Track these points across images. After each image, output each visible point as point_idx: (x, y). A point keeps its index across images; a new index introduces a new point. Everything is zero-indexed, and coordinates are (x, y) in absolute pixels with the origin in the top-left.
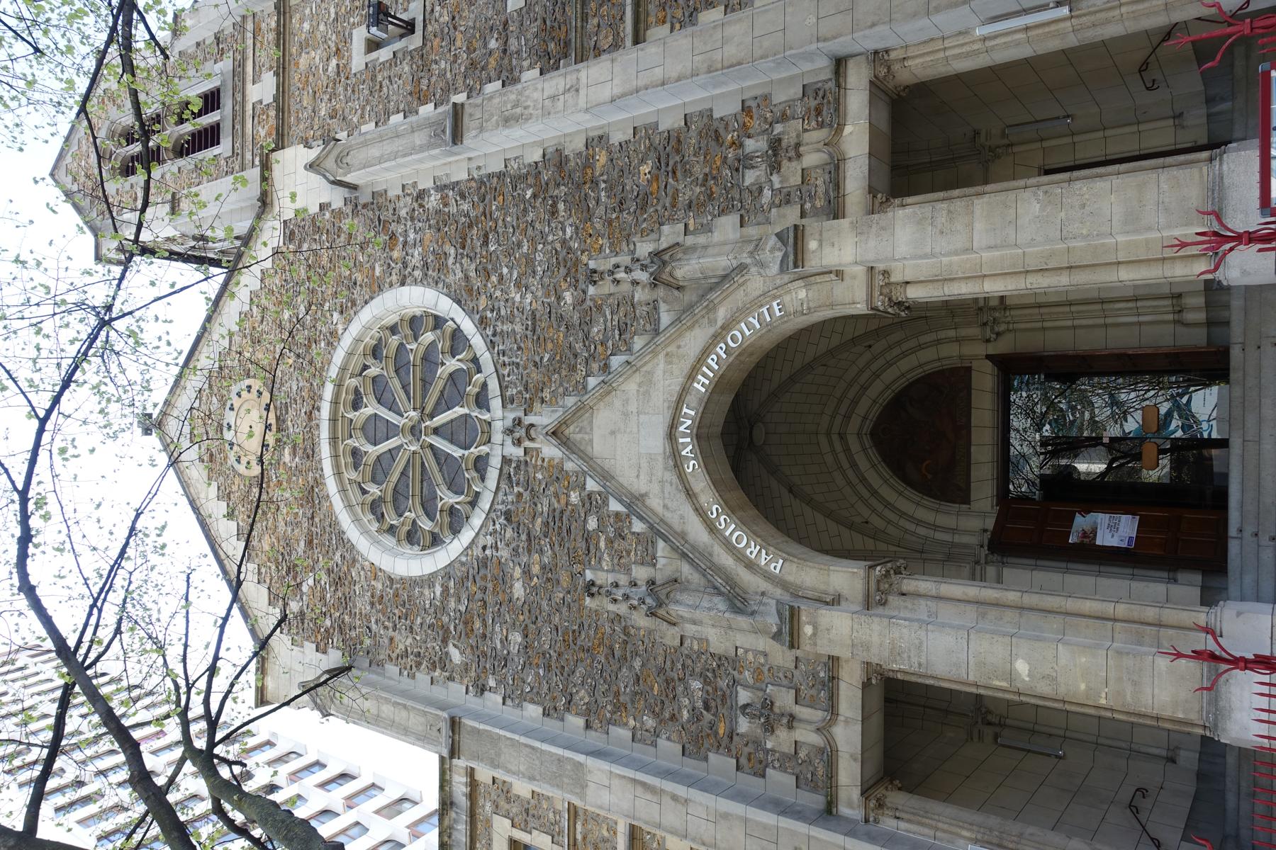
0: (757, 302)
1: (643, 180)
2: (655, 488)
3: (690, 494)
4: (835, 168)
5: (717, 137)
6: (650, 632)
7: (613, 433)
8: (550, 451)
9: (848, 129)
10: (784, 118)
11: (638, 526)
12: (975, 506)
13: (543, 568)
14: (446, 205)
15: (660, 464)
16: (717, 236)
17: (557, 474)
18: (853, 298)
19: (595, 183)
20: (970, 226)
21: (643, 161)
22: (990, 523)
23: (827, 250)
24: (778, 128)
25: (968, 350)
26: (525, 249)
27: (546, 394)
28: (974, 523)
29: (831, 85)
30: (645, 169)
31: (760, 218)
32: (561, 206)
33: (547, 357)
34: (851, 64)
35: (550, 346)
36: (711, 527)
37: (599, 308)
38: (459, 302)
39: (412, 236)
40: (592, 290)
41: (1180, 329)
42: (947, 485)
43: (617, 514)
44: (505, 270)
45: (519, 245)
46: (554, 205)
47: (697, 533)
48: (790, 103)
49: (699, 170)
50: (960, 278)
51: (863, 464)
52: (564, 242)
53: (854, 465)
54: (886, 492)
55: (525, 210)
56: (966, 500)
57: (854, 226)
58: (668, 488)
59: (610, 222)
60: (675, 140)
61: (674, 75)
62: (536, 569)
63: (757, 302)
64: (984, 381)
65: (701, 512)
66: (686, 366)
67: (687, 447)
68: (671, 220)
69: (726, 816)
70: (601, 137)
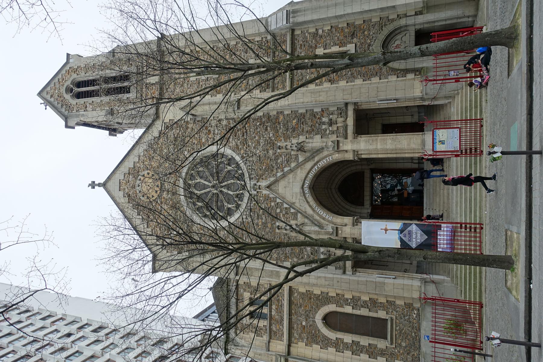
0: (326, 157)
1: (294, 124)
2: (298, 201)
3: (308, 202)
4: (346, 127)
5: (315, 116)
6: (296, 237)
7: (285, 187)
8: (265, 192)
9: (348, 119)
10: (332, 114)
11: (292, 210)
12: (365, 207)
13: (263, 223)
14: (229, 124)
15: (299, 195)
16: (315, 140)
17: (267, 198)
18: (350, 156)
19: (279, 123)
20: (377, 143)
21: (294, 119)
22: (369, 211)
23: (345, 146)
24: (331, 116)
25: (363, 167)
26: (257, 138)
27: (264, 177)
28: (366, 211)
29: (344, 108)
30: (294, 121)
31: (326, 137)
32: (269, 128)
33: (264, 167)
34: (349, 104)
35: (265, 164)
36: (313, 210)
37: (281, 156)
38: (234, 151)
39: (216, 131)
40: (279, 151)
41: (413, 164)
42: (359, 202)
43: (286, 208)
44: (250, 144)
45: (255, 137)
46: (267, 128)
47: (310, 211)
48: (334, 111)
49: (310, 124)
50: (226, 83)
51: (336, 196)
52: (269, 138)
53: (334, 197)
54: (342, 203)
55: (257, 128)
56: (363, 205)
57: (351, 141)
58: (301, 201)
59: (284, 134)
60: (303, 115)
61: (306, 101)
62: (260, 224)
63: (326, 157)
64: (367, 175)
65: (310, 206)
66: (307, 172)
67: (307, 190)
68: (302, 135)
69: (320, 277)
70: (281, 112)
